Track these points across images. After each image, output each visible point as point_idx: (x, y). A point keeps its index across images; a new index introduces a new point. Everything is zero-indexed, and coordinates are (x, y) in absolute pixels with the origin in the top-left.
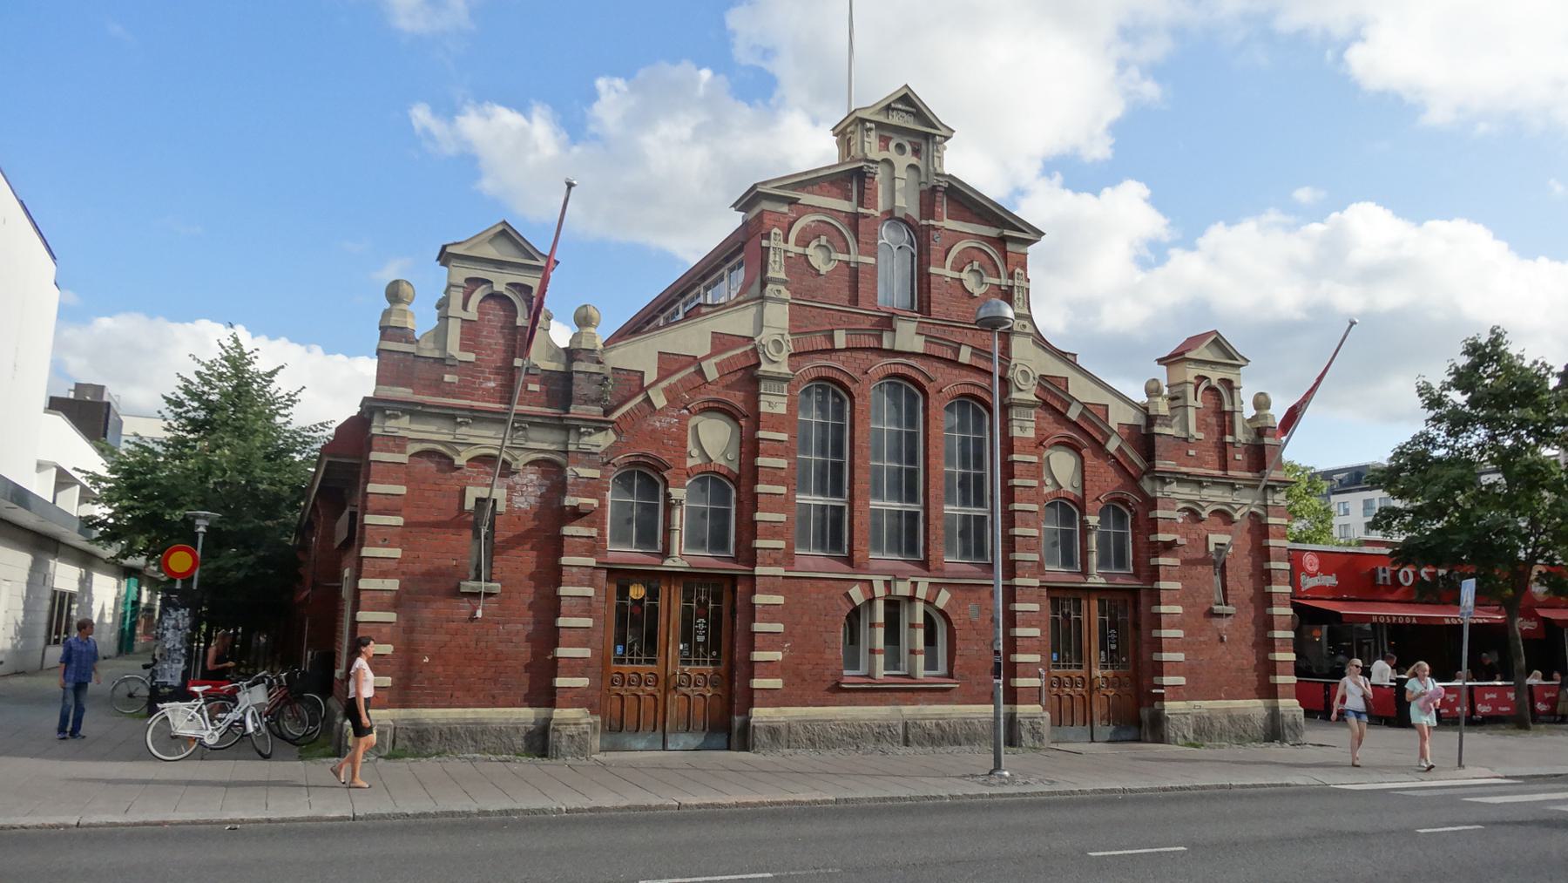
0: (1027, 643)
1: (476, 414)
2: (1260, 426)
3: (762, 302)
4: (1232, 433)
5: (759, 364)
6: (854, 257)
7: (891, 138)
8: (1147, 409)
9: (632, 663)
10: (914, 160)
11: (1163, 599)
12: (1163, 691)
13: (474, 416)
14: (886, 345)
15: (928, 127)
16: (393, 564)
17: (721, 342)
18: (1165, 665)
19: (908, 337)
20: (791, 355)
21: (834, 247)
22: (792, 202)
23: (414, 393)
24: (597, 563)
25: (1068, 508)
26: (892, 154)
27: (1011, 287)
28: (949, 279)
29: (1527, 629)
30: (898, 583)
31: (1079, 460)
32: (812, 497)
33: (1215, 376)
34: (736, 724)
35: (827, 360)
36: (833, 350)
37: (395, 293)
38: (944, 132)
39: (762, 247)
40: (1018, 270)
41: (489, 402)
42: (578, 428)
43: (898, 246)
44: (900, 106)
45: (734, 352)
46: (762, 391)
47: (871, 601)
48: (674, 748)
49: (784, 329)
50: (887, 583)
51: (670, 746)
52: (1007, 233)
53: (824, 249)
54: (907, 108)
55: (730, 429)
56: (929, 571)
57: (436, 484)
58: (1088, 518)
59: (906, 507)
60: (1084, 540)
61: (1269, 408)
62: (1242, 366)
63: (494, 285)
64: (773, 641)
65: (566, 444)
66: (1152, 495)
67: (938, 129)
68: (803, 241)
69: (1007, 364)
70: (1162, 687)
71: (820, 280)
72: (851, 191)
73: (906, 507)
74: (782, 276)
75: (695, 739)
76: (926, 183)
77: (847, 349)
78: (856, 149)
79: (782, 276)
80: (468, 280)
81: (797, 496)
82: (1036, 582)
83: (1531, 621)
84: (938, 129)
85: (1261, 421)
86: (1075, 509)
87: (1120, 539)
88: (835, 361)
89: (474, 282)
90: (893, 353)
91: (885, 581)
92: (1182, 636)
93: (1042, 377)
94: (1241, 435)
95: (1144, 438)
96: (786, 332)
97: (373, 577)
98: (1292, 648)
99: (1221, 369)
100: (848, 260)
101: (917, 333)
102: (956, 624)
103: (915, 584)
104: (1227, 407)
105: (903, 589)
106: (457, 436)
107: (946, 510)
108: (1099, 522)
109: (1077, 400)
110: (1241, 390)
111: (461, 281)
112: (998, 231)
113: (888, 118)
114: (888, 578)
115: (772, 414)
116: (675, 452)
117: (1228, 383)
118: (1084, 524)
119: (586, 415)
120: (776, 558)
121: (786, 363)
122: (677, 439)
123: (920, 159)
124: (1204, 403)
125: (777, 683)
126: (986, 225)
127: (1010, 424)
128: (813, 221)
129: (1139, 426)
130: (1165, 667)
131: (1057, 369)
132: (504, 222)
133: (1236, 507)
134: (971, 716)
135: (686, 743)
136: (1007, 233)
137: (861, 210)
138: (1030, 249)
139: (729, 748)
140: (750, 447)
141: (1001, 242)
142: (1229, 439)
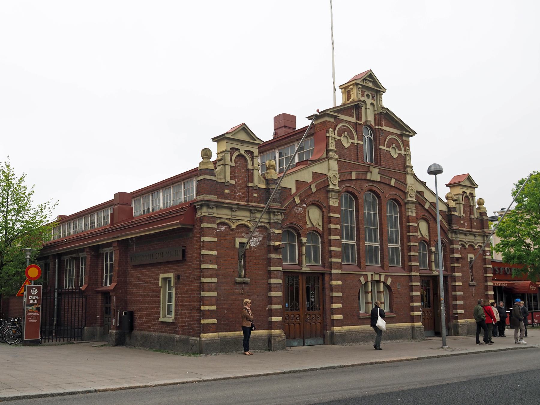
0: (416, 298)
1: (240, 207)
2: (481, 211)
3: (328, 160)
4: (252, 181)
5: (328, 186)
6: (356, 141)
7: (365, 92)
8: (448, 205)
9: (291, 311)
10: (372, 101)
11: (456, 280)
12: (457, 316)
13: (239, 208)
14: (368, 178)
15: (378, 88)
16: (214, 272)
17: (316, 175)
18: (458, 306)
19: (375, 175)
20: (339, 182)
21: (350, 136)
22: (335, 117)
23: (217, 198)
24: (282, 269)
25: (426, 243)
26: (365, 98)
27: (405, 155)
28: (386, 151)
29: (533, 290)
30: (376, 275)
31: (321, 213)
32: (368, 243)
33: (468, 191)
34: (328, 334)
35: (349, 184)
36: (352, 180)
37: (505, 209)
38: (383, 90)
39: (327, 136)
40: (407, 148)
41: (239, 201)
42: (274, 212)
43: (367, 137)
44: (368, 79)
45: (321, 181)
46: (331, 197)
47: (367, 282)
48: (306, 345)
49: (336, 171)
50: (372, 275)
51: (305, 344)
52: (405, 133)
53: (345, 137)
54: (370, 79)
55: (319, 212)
56: (384, 270)
57: (224, 237)
58: (302, 238)
59: (375, 244)
60: (430, 257)
61: (483, 204)
62: (476, 188)
63: (241, 151)
64: (338, 300)
65: (269, 219)
66: (451, 239)
67: (382, 89)
68: (340, 135)
69: (406, 186)
70: (457, 314)
71: (345, 151)
72: (353, 113)
73: (375, 244)
74: (335, 149)
75: (313, 341)
76: (377, 111)
77: (356, 179)
78: (354, 96)
79: (335, 149)
80: (231, 149)
81: (342, 240)
82: (418, 274)
83: (534, 287)
84: (382, 89)
85: (482, 210)
86: (319, 236)
87: (316, 248)
88: (351, 184)
89: (234, 150)
90: (371, 181)
91: (371, 274)
92: (462, 294)
93: (417, 192)
94: (476, 215)
95: (449, 216)
96: (337, 172)
97: (208, 277)
98: (493, 298)
99: (470, 189)
100: (354, 142)
101: (378, 173)
102: (394, 291)
103: (380, 275)
104: (250, 167)
105: (377, 278)
106: (232, 216)
107: (389, 245)
108: (307, 240)
109: (428, 201)
110: (476, 197)
111: (229, 149)
112: (401, 131)
113: (364, 83)
114: (372, 273)
115: (334, 206)
116: (302, 222)
117: (471, 194)
118: (300, 241)
119: (276, 207)
120: (340, 266)
121: (337, 185)
122: (303, 217)
123: (374, 100)
124: (236, 163)
125: (340, 317)
126: (396, 129)
127: (407, 210)
128: (342, 126)
129: (446, 211)
130: (458, 306)
131: (421, 189)
132: (244, 124)
133: (476, 243)
134: (400, 328)
135: (310, 343)
136: (405, 133)
137: (358, 121)
138: (411, 138)
139: (324, 344)
140: (327, 220)
141: (401, 136)
142: (472, 217)
